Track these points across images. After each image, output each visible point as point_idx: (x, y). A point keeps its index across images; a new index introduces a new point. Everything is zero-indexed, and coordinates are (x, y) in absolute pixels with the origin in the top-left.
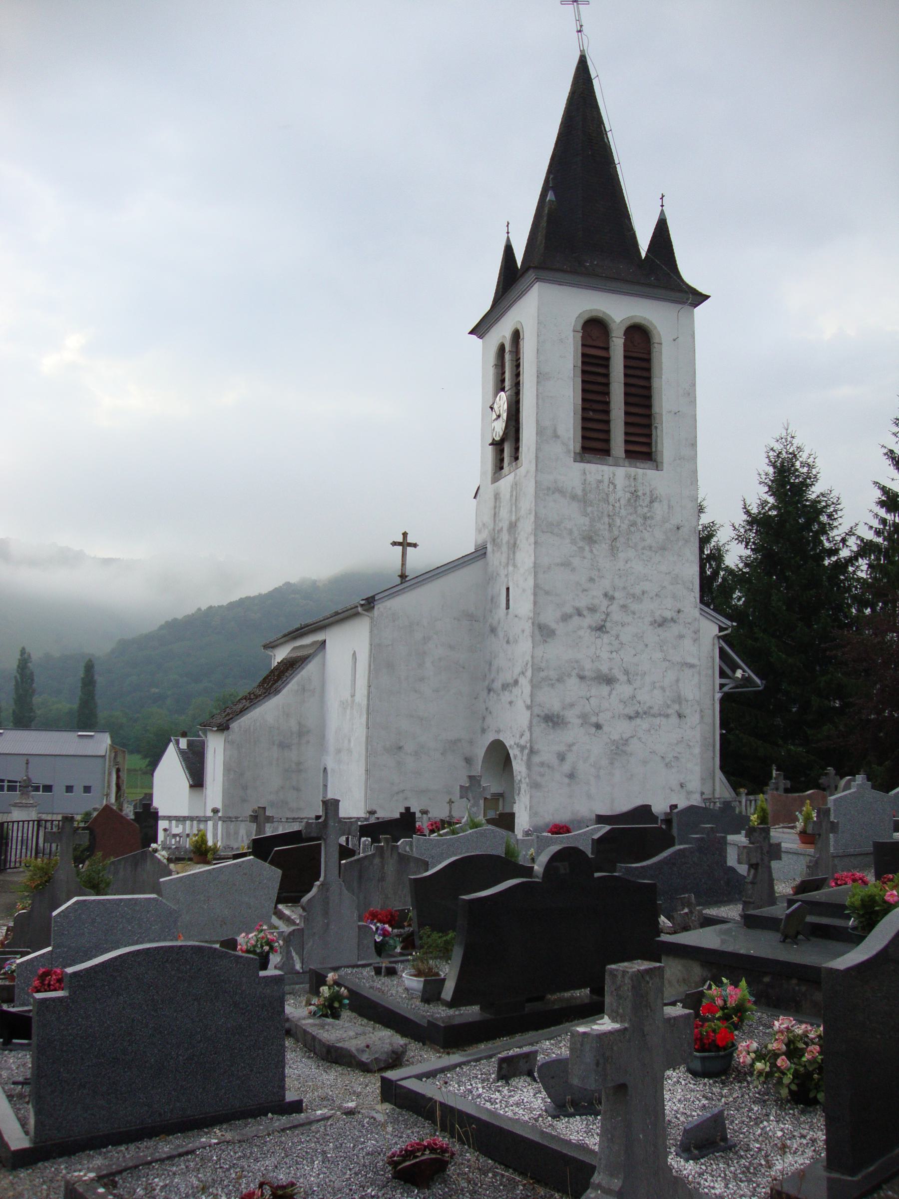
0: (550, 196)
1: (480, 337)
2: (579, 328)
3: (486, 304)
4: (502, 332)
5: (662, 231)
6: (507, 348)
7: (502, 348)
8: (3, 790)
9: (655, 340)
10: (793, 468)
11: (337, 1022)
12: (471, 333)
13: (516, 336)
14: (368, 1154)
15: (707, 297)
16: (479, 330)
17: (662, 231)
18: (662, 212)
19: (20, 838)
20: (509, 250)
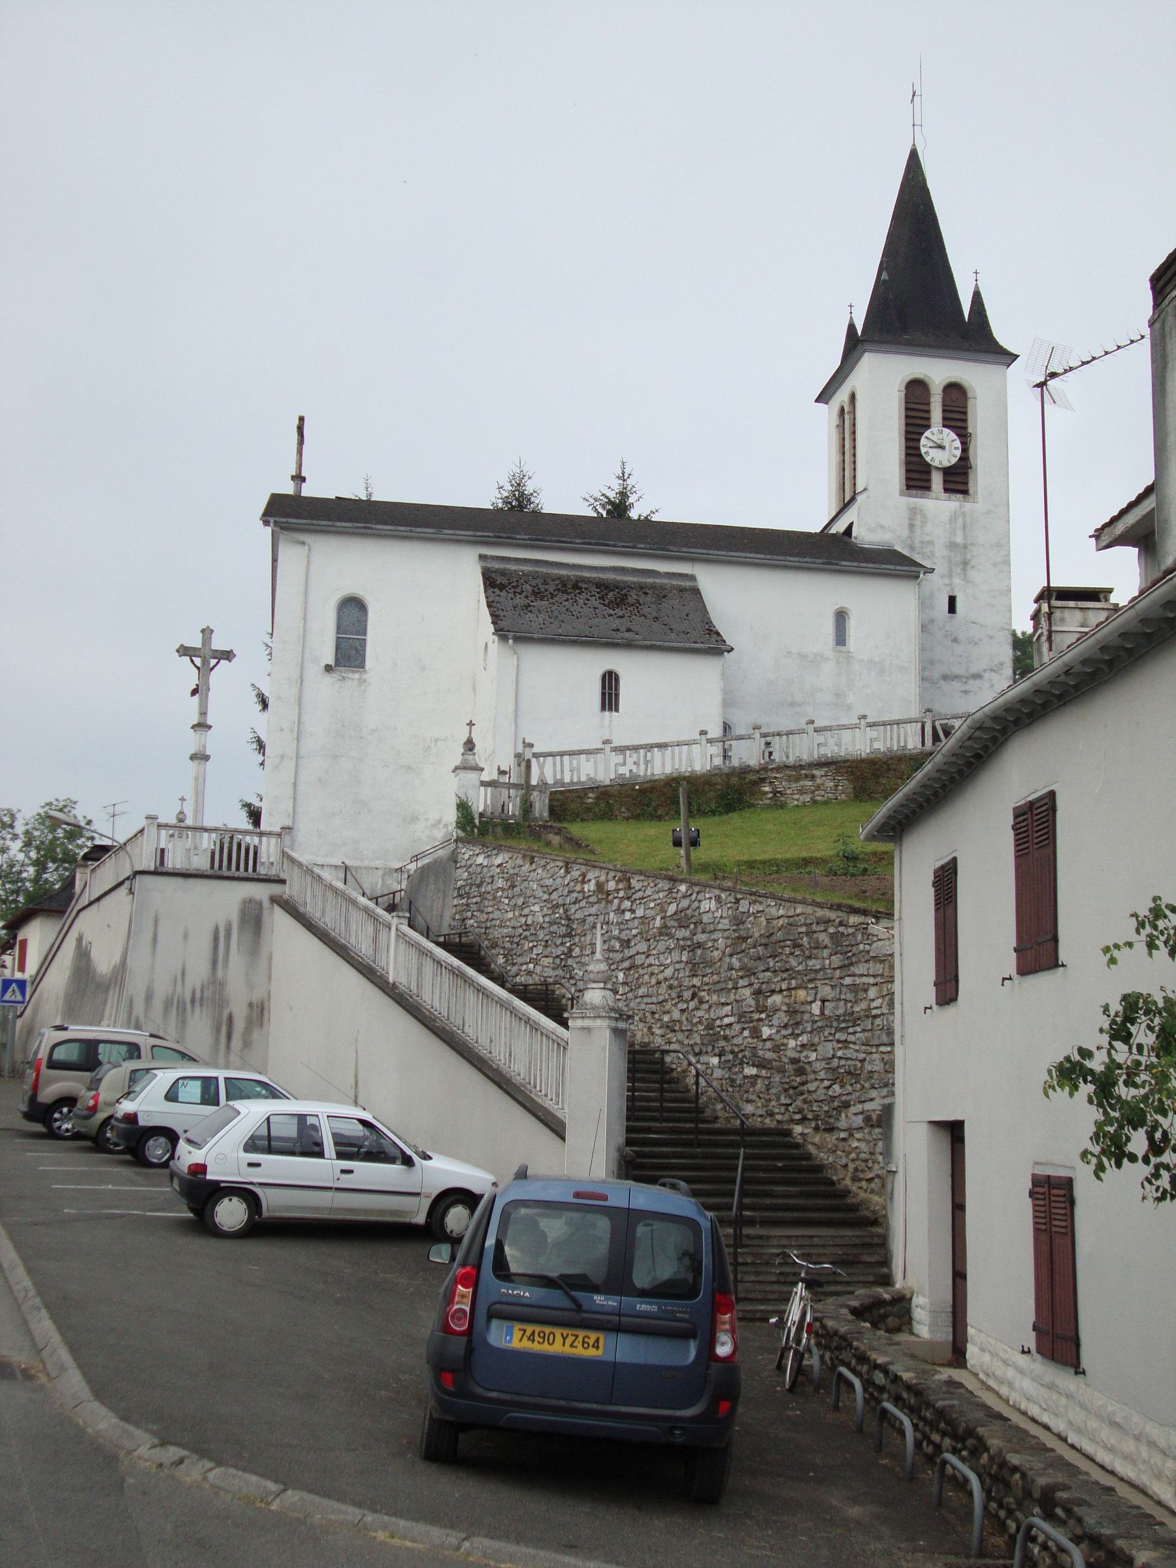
0: (885, 276)
1: (826, 403)
2: (903, 388)
3: (834, 361)
4: (842, 397)
5: (977, 297)
6: (846, 410)
7: (842, 410)
8: (1012, 1566)
9: (970, 395)
10: (258, 1504)
11: (968, 506)
12: (817, 401)
13: (853, 397)
14: (568, 594)
15: (1017, 356)
16: (824, 397)
17: (977, 297)
18: (977, 285)
19: (802, 1202)
20: (851, 327)
